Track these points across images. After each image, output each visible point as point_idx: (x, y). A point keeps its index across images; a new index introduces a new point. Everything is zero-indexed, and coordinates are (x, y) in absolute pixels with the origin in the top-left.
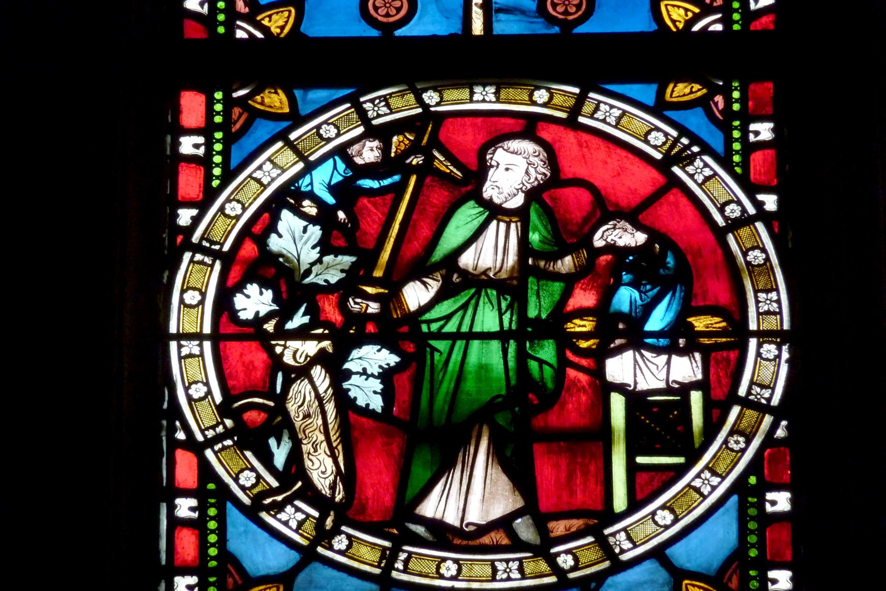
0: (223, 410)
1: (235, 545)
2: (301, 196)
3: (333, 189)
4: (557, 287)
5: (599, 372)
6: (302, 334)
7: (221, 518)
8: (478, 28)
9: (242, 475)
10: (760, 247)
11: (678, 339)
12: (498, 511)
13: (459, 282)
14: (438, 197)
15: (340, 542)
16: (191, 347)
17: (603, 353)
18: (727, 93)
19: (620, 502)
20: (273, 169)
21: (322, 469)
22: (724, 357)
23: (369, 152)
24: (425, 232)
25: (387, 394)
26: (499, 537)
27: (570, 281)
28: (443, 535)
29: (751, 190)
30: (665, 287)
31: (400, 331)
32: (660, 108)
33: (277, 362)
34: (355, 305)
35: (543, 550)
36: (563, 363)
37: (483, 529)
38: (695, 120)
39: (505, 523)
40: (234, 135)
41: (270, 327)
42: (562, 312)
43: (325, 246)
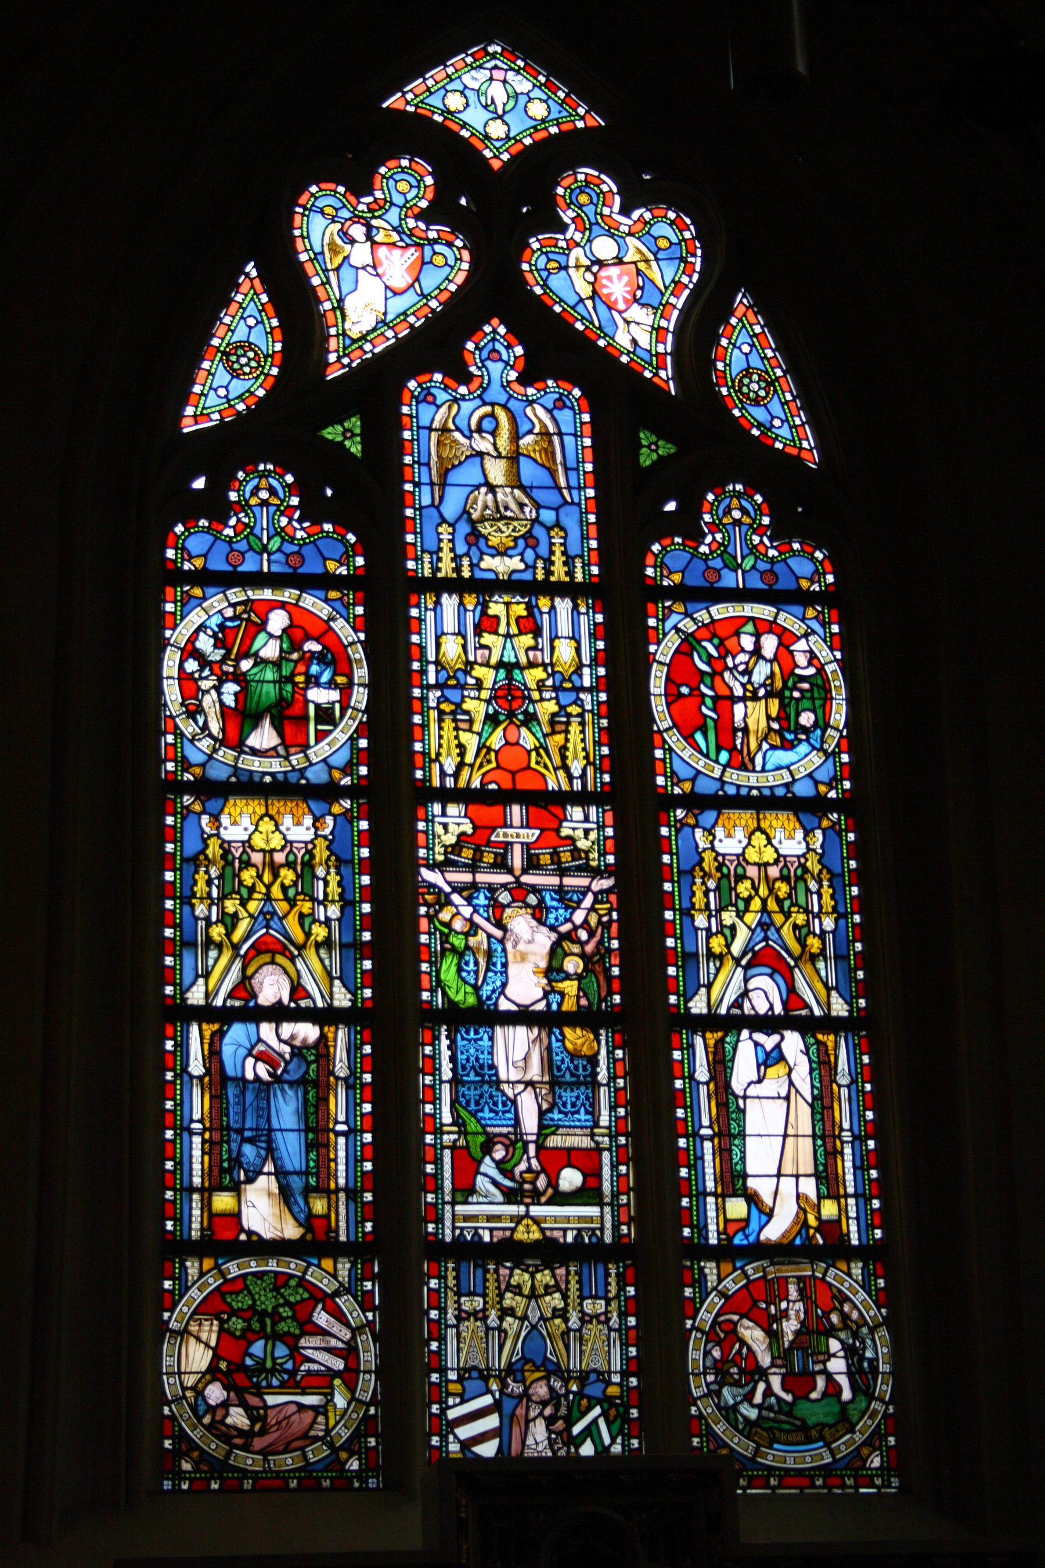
0: (182, 704)
1: (675, 768)
2: (206, 627)
3: (218, 626)
4: (292, 664)
5: (305, 696)
6: (206, 678)
7: (671, 758)
8: (265, 570)
9: (189, 728)
10: (358, 653)
11: (331, 684)
12: (273, 744)
13: (260, 662)
14: (253, 629)
15: (221, 753)
16: (171, 681)
17: (306, 689)
18: (348, 595)
19: (312, 741)
20: (196, 617)
21: (215, 727)
22: (346, 691)
23: (229, 613)
24: (248, 642)
25: (236, 701)
26: (273, 753)
27: (296, 662)
28: (254, 752)
29: (356, 631)
30: (328, 665)
31: (238, 677)
32: (326, 600)
33: (199, 688)
34: (225, 668)
35: (286, 758)
36: (294, 692)
37: (267, 750)
38: (338, 605)
39: (274, 748)
40: (186, 603)
41: (196, 675)
42: (293, 674)
43: (215, 646)
